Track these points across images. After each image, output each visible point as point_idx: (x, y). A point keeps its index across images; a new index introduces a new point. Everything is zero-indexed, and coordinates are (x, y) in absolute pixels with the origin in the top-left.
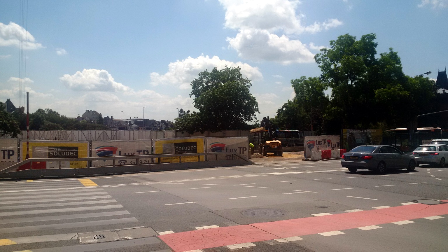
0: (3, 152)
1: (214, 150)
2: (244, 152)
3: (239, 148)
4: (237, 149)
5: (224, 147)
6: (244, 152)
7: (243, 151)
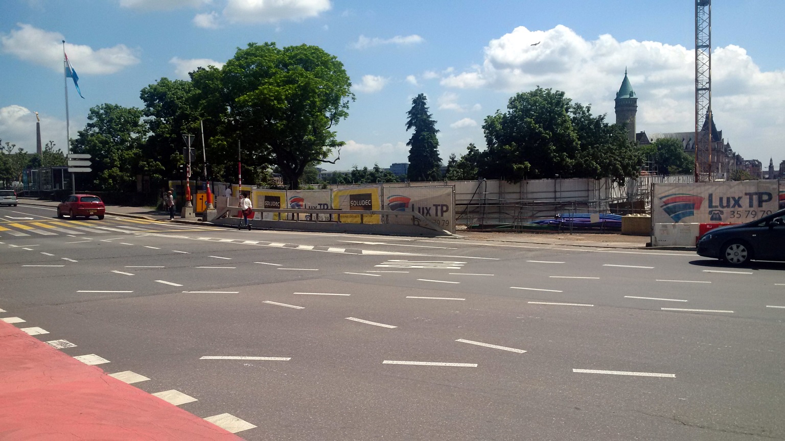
0: (748, 197)
1: (393, 208)
2: (445, 214)
3: (319, 204)
4: (430, 208)
5: (408, 203)
6: (445, 214)
7: (442, 212)
